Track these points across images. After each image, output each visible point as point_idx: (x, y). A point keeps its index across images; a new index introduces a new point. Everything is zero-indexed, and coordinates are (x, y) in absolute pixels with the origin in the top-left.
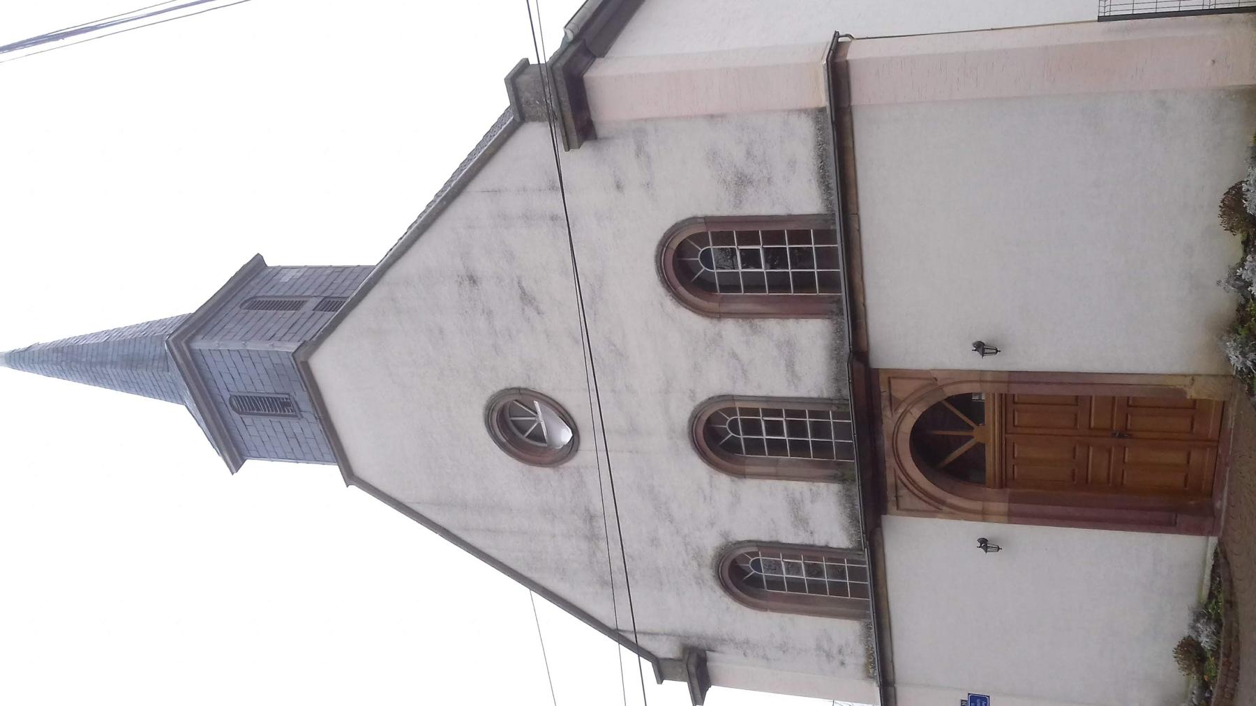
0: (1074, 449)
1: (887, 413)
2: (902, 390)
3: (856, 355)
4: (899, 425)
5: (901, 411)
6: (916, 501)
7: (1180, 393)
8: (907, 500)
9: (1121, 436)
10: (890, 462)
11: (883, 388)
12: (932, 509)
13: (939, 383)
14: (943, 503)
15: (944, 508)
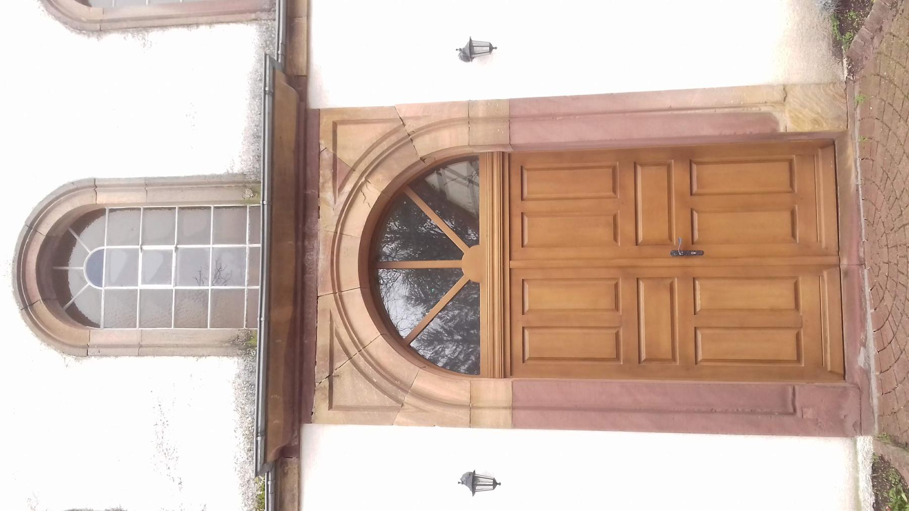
0: (616, 286)
1: (327, 194)
2: (353, 145)
3: (287, 78)
4: (344, 217)
5: (348, 188)
6: (362, 384)
7: (767, 119)
8: (350, 387)
9: (686, 253)
10: (326, 301)
11: (325, 143)
12: (389, 402)
13: (411, 126)
14: (405, 387)
15: (408, 399)
